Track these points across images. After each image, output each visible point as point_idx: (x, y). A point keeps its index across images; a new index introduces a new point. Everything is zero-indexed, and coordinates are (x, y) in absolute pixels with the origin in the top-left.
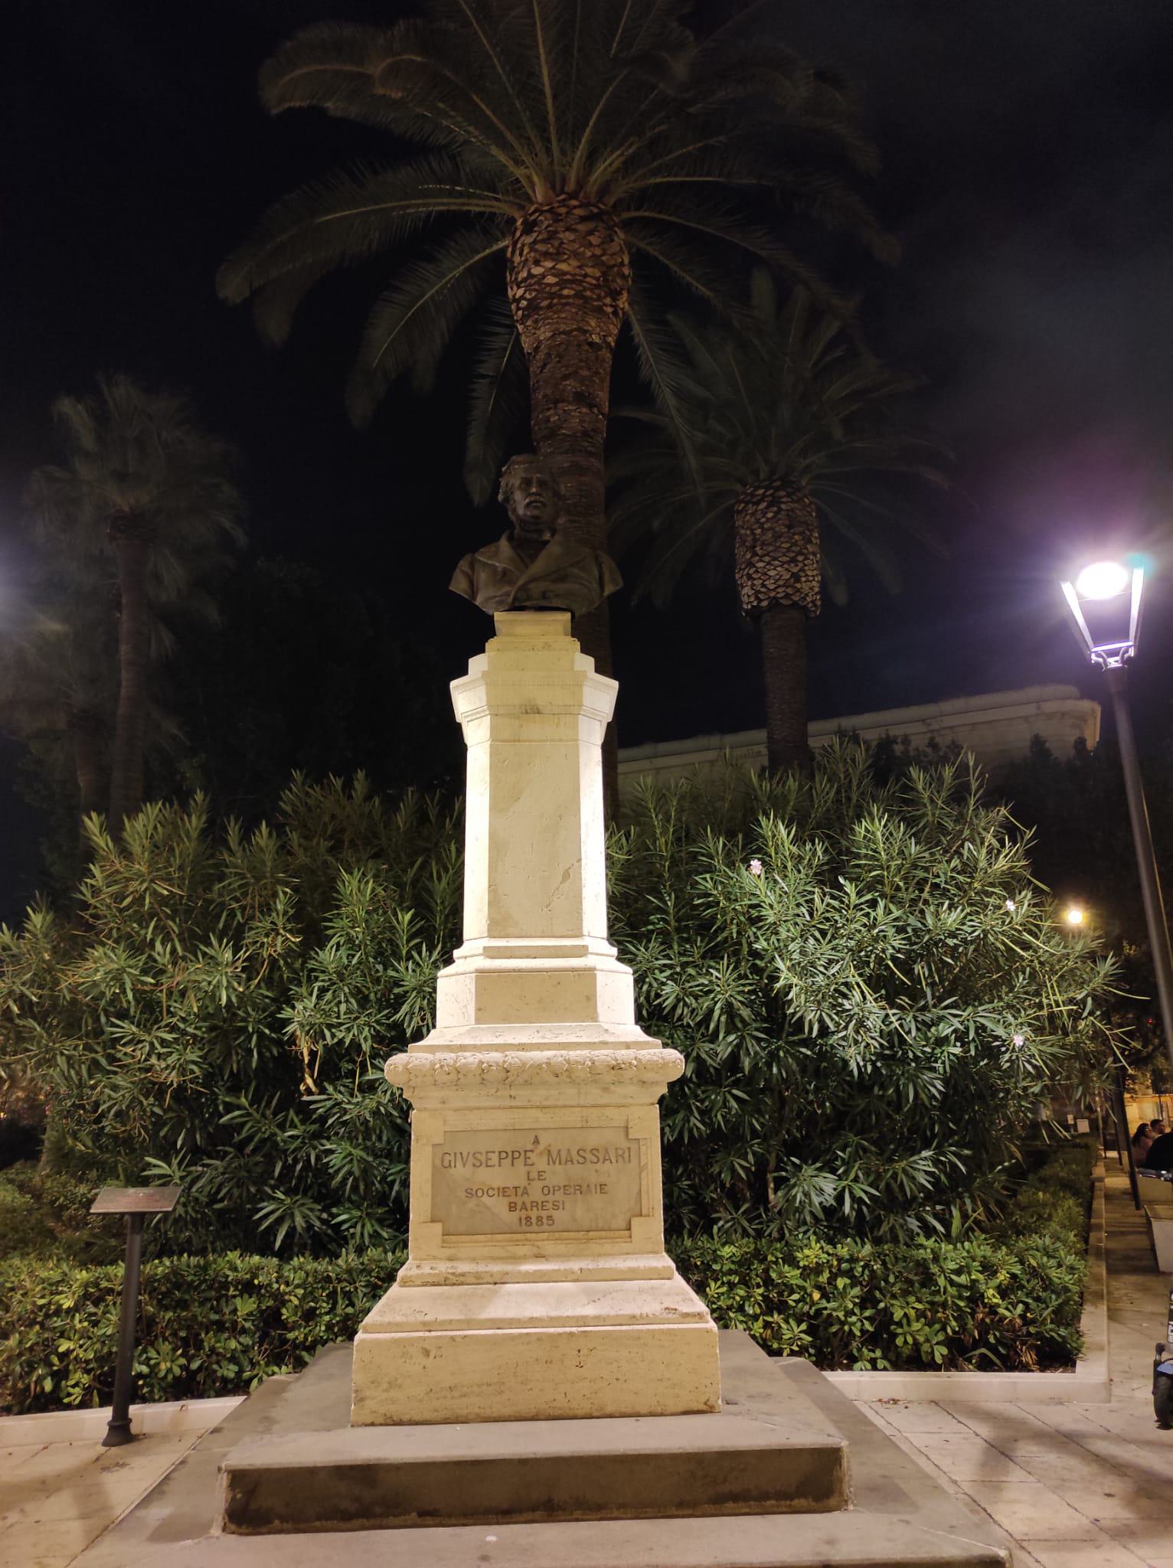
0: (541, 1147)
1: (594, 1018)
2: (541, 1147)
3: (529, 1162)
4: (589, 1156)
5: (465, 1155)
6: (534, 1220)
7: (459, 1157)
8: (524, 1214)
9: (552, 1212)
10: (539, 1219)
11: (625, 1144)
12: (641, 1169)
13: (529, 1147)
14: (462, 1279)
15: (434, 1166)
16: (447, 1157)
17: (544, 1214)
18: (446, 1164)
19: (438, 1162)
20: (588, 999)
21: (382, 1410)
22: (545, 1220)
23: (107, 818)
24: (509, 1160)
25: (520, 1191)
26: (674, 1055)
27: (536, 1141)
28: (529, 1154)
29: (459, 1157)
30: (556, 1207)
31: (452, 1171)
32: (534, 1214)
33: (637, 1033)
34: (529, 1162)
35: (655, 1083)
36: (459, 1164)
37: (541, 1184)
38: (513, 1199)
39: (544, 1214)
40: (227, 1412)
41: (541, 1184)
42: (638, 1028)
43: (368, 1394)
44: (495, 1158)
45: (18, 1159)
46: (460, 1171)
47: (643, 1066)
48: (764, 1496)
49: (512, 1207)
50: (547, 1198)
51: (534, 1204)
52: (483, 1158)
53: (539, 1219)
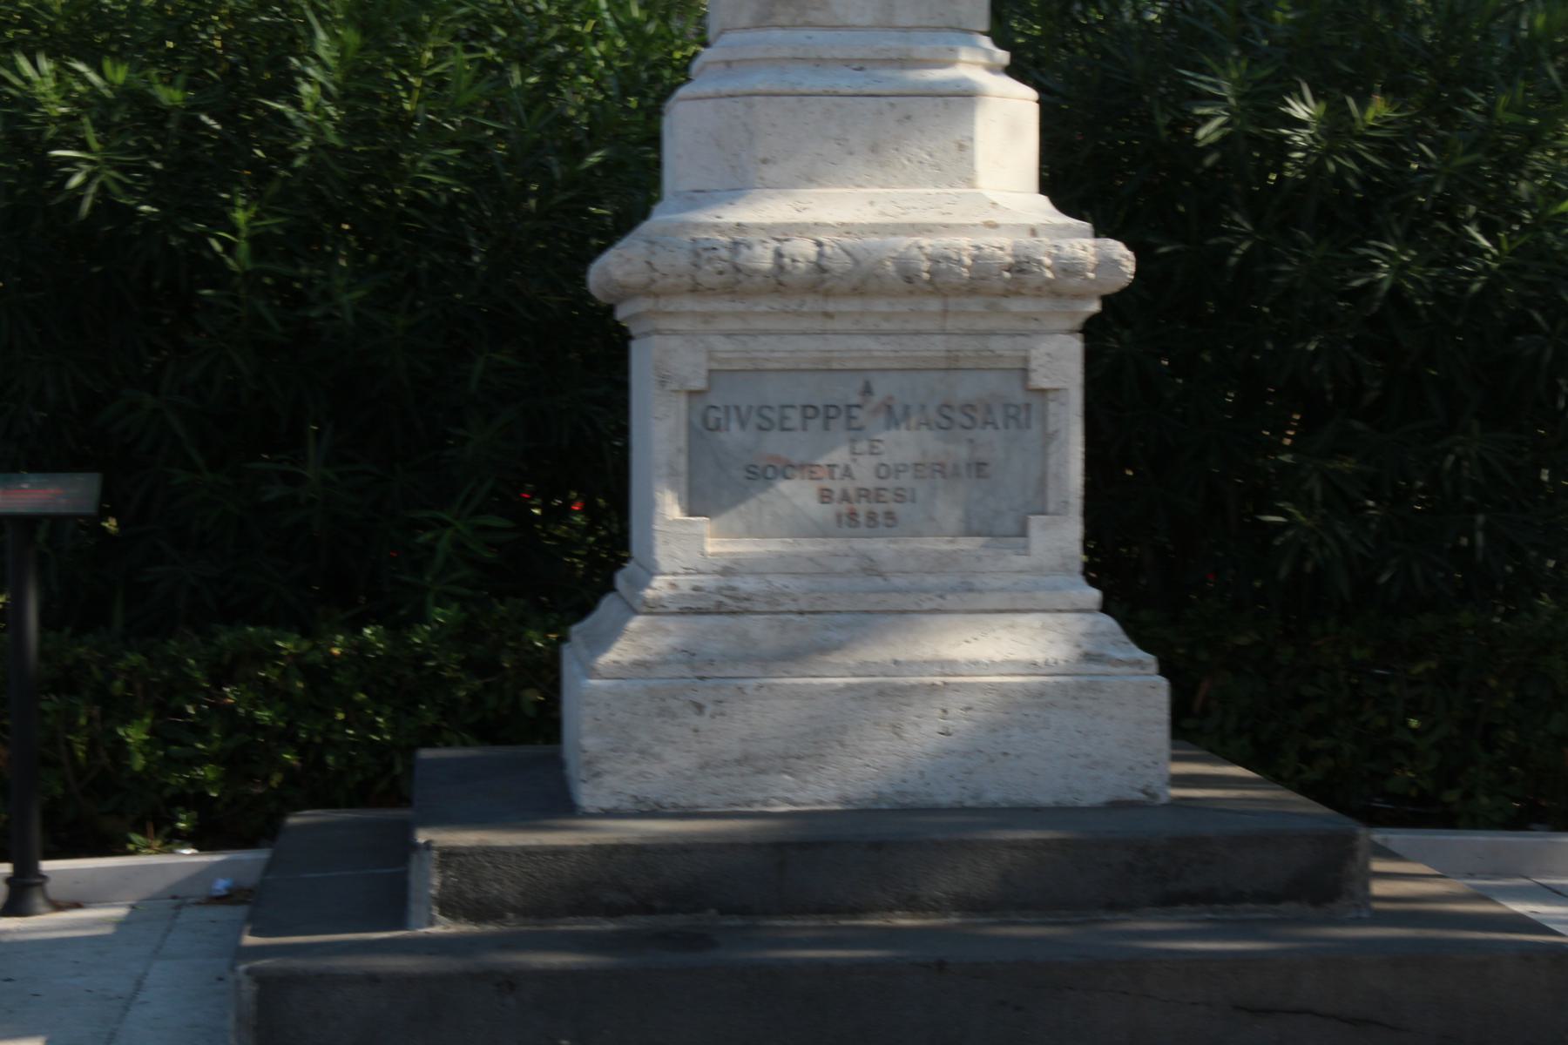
0: (877, 399)
1: (970, 181)
2: (877, 399)
3: (855, 424)
4: (959, 417)
5: (743, 409)
6: (862, 519)
7: (733, 414)
8: (844, 508)
9: (894, 506)
10: (872, 516)
11: (1019, 397)
12: (1048, 438)
13: (855, 400)
14: (746, 605)
15: (690, 426)
16: (713, 414)
17: (879, 509)
18: (712, 424)
19: (697, 421)
20: (961, 147)
21: (632, 789)
22: (880, 519)
23: (1329, 110)
24: (842, 418)
25: (838, 472)
26: (1119, 250)
27: (867, 391)
28: (855, 412)
29: (733, 414)
30: (900, 496)
31: (722, 436)
32: (862, 508)
33: (1042, 210)
34: (855, 424)
35: (1080, 296)
36: (734, 426)
37: (874, 460)
38: (827, 483)
39: (879, 509)
40: (159, 885)
41: (874, 460)
42: (1044, 201)
43: (605, 766)
44: (795, 418)
45: (1137, 274)
46: (734, 436)
47: (1068, 269)
48: (1237, 897)
49: (825, 496)
50: (883, 483)
51: (864, 493)
52: (774, 416)
53: (872, 516)
